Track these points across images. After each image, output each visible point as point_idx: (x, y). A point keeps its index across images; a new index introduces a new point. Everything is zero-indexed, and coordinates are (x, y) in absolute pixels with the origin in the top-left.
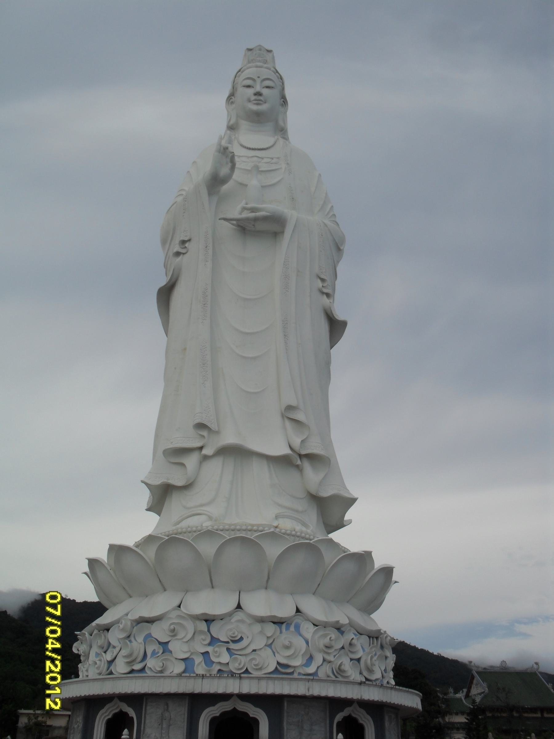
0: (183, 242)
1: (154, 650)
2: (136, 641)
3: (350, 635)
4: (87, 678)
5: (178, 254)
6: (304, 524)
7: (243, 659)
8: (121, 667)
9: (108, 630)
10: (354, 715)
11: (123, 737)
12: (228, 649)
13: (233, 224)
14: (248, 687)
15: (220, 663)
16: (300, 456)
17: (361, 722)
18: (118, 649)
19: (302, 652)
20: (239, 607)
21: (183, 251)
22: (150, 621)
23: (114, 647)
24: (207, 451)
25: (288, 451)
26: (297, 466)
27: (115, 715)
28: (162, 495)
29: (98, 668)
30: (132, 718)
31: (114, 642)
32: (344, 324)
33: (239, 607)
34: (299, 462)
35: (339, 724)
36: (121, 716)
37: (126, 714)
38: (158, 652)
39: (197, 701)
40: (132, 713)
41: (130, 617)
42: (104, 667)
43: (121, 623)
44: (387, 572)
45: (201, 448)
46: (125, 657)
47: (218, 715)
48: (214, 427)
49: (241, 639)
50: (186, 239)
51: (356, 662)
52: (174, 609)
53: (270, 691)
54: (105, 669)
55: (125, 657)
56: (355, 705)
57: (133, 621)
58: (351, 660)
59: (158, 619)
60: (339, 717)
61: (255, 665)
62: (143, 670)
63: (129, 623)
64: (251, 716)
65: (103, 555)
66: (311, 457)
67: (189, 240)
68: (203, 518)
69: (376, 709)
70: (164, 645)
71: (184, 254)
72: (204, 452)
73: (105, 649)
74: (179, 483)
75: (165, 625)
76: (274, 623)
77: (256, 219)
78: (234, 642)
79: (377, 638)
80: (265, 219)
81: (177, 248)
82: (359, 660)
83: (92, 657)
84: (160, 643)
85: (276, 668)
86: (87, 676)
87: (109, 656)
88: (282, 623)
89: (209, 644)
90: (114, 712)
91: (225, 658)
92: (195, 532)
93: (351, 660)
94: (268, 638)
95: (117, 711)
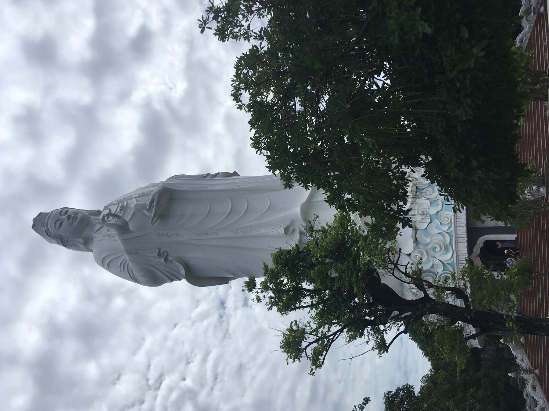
0: (159, 254)
21: (166, 254)
23: (433, 266)
62: (451, 237)
67: (159, 250)
71: (167, 255)
77: (158, 203)
81: (163, 260)
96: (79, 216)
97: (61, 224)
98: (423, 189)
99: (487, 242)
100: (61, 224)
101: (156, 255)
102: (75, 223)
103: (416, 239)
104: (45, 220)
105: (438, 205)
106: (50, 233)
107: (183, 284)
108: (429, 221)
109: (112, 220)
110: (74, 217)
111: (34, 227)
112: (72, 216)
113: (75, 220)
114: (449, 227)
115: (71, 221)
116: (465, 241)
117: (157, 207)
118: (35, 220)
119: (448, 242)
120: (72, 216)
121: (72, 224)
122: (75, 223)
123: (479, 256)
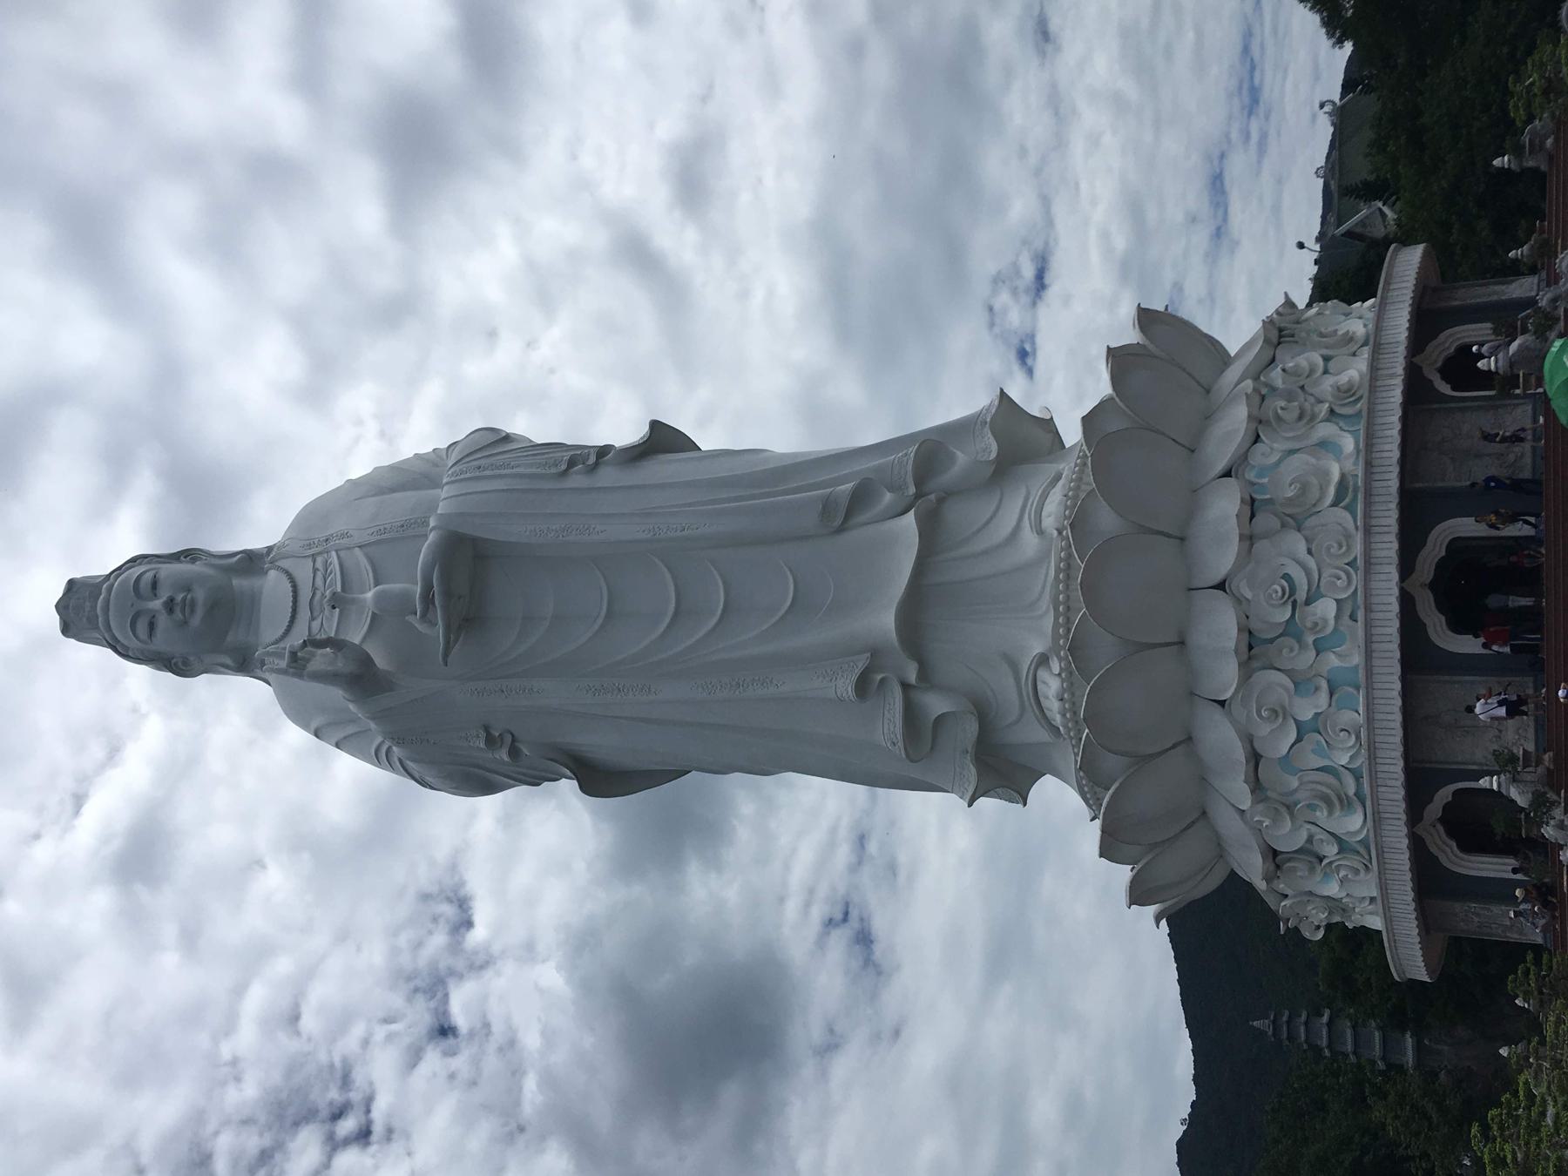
0: (491, 741)
1: (1313, 751)
2: (1296, 790)
3: (1276, 376)
4: (1379, 901)
5: (514, 752)
6: (1058, 477)
7: (1326, 573)
8: (1353, 823)
9: (1275, 853)
10: (1439, 364)
11: (1495, 787)
12: (1308, 602)
13: (456, 642)
14: (1388, 548)
15: (1337, 617)
16: (919, 495)
17: (1434, 850)
18: (1314, 829)
19: (1313, 460)
20: (1221, 586)
21: (508, 739)
22: (1255, 758)
23: (1310, 839)
24: (912, 678)
25: (910, 518)
26: (941, 501)
27: (1451, 833)
28: (1002, 772)
29: (1357, 872)
30: (1456, 793)
31: (1300, 840)
32: (656, 426)
33: (1221, 586)
34: (932, 497)
35: (1454, 389)
36: (1453, 817)
37: (1446, 807)
38: (1318, 743)
39: (1417, 656)
40: (1445, 794)
41: (1246, 805)
42: (1353, 861)
43: (1261, 822)
44: (1146, 318)
45: (906, 686)
46: (1331, 813)
47: (1443, 619)
48: (861, 663)
49: (1286, 577)
50: (483, 734)
51: (1331, 364)
52: (1229, 714)
53: (1394, 515)
54: (1356, 880)
55: (1331, 813)
56: (1419, 830)
57: (1256, 802)
58: (1326, 372)
59: (1249, 740)
60: (1445, 388)
61: (1340, 546)
62: (1358, 777)
63: (1260, 807)
64: (1443, 553)
65: (1123, 874)
66: (920, 480)
67: (487, 729)
68: (1043, 674)
69: (1425, 323)
70: (1302, 730)
71: (514, 741)
72: (912, 678)
73: (1314, 860)
74: (972, 728)
75: (1263, 730)
76: (1253, 516)
77: (447, 594)
78: (1293, 590)
79: (1281, 330)
80: (446, 577)
81: (503, 755)
82: (1327, 359)
83: (1333, 889)
84: (1299, 740)
85: (1345, 508)
86: (1372, 900)
87: (1331, 850)
88: (1253, 500)
89: (1299, 639)
90: (1444, 836)
91: (1326, 608)
92: (1071, 673)
93: (1326, 372)
94: (1283, 525)
95: (1440, 828)
96: (200, 595)
97: (152, 626)
98: (1272, 641)
99: (1457, 546)
100: (152, 626)
101: (482, 745)
102: (196, 621)
103: (1257, 779)
104: (94, 607)
105: (1317, 689)
106: (127, 648)
107: (567, 787)
108: (1293, 736)
109: (321, 660)
110: (184, 599)
111: (67, 630)
112: (179, 597)
113: (193, 611)
114: (1351, 757)
115: (178, 615)
116: (1402, 823)
117: (445, 608)
118: (61, 607)
119: (1351, 791)
120: (179, 597)
121: (185, 623)
122: (196, 621)
123: (1441, 820)
